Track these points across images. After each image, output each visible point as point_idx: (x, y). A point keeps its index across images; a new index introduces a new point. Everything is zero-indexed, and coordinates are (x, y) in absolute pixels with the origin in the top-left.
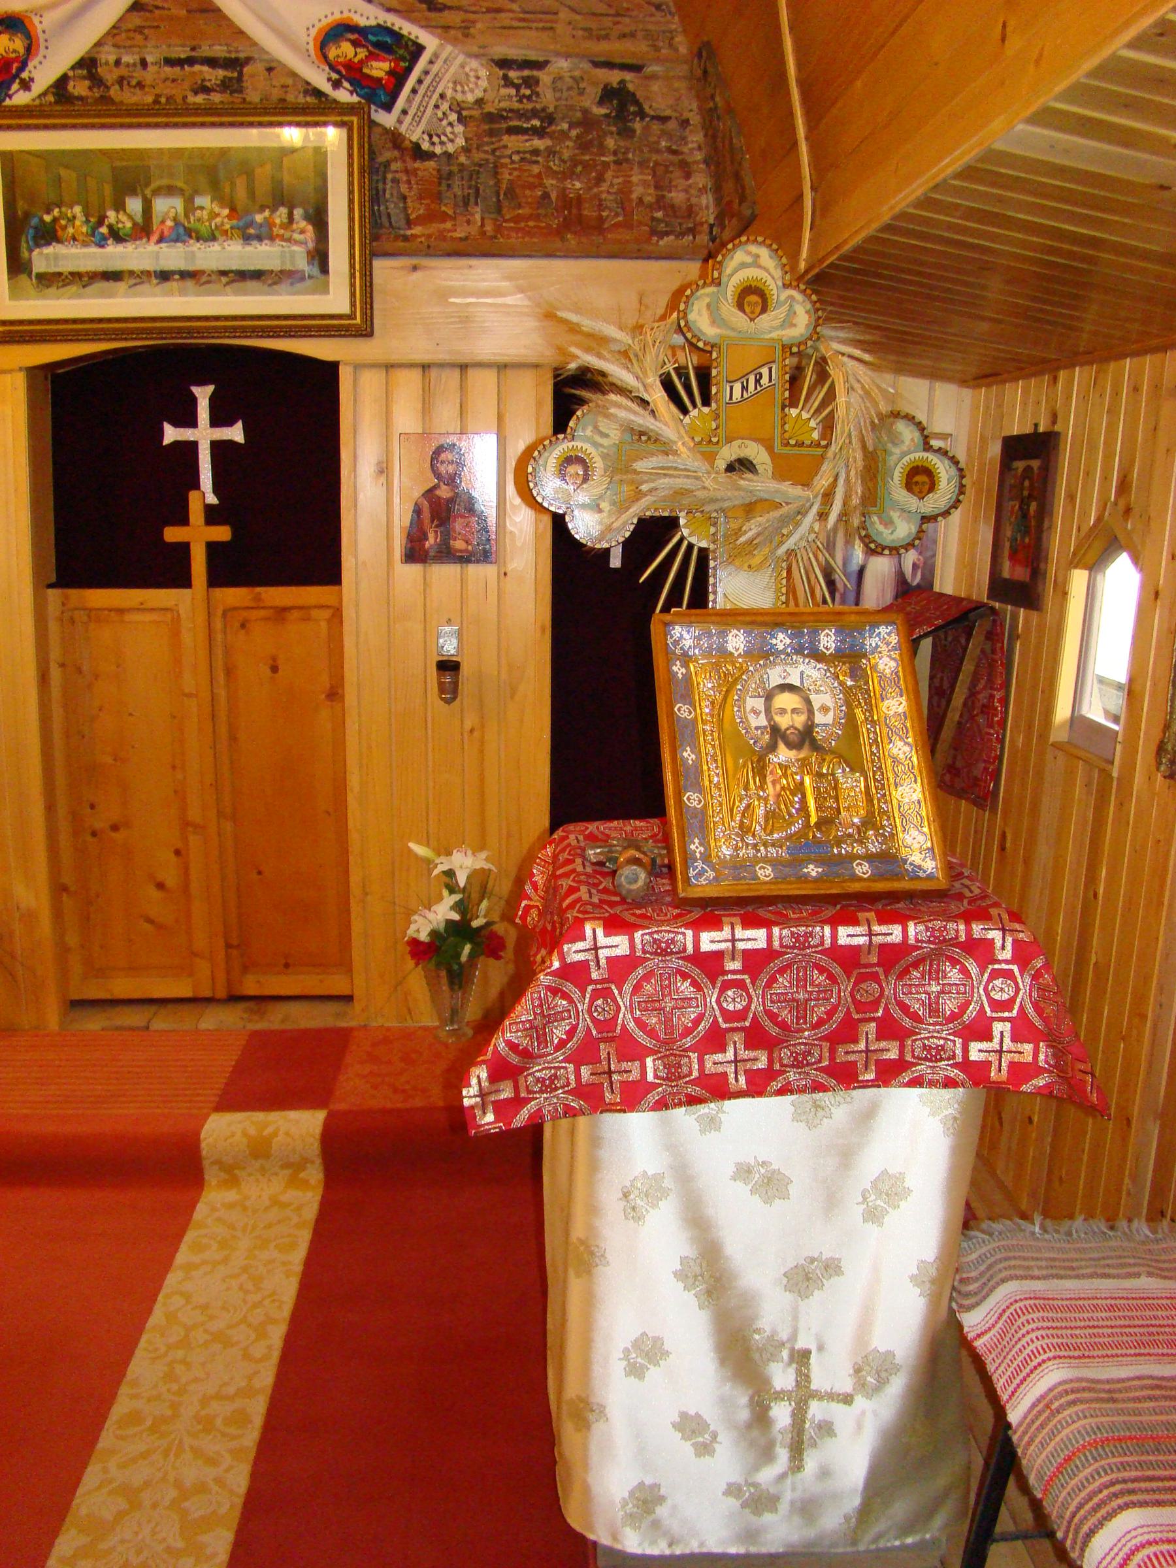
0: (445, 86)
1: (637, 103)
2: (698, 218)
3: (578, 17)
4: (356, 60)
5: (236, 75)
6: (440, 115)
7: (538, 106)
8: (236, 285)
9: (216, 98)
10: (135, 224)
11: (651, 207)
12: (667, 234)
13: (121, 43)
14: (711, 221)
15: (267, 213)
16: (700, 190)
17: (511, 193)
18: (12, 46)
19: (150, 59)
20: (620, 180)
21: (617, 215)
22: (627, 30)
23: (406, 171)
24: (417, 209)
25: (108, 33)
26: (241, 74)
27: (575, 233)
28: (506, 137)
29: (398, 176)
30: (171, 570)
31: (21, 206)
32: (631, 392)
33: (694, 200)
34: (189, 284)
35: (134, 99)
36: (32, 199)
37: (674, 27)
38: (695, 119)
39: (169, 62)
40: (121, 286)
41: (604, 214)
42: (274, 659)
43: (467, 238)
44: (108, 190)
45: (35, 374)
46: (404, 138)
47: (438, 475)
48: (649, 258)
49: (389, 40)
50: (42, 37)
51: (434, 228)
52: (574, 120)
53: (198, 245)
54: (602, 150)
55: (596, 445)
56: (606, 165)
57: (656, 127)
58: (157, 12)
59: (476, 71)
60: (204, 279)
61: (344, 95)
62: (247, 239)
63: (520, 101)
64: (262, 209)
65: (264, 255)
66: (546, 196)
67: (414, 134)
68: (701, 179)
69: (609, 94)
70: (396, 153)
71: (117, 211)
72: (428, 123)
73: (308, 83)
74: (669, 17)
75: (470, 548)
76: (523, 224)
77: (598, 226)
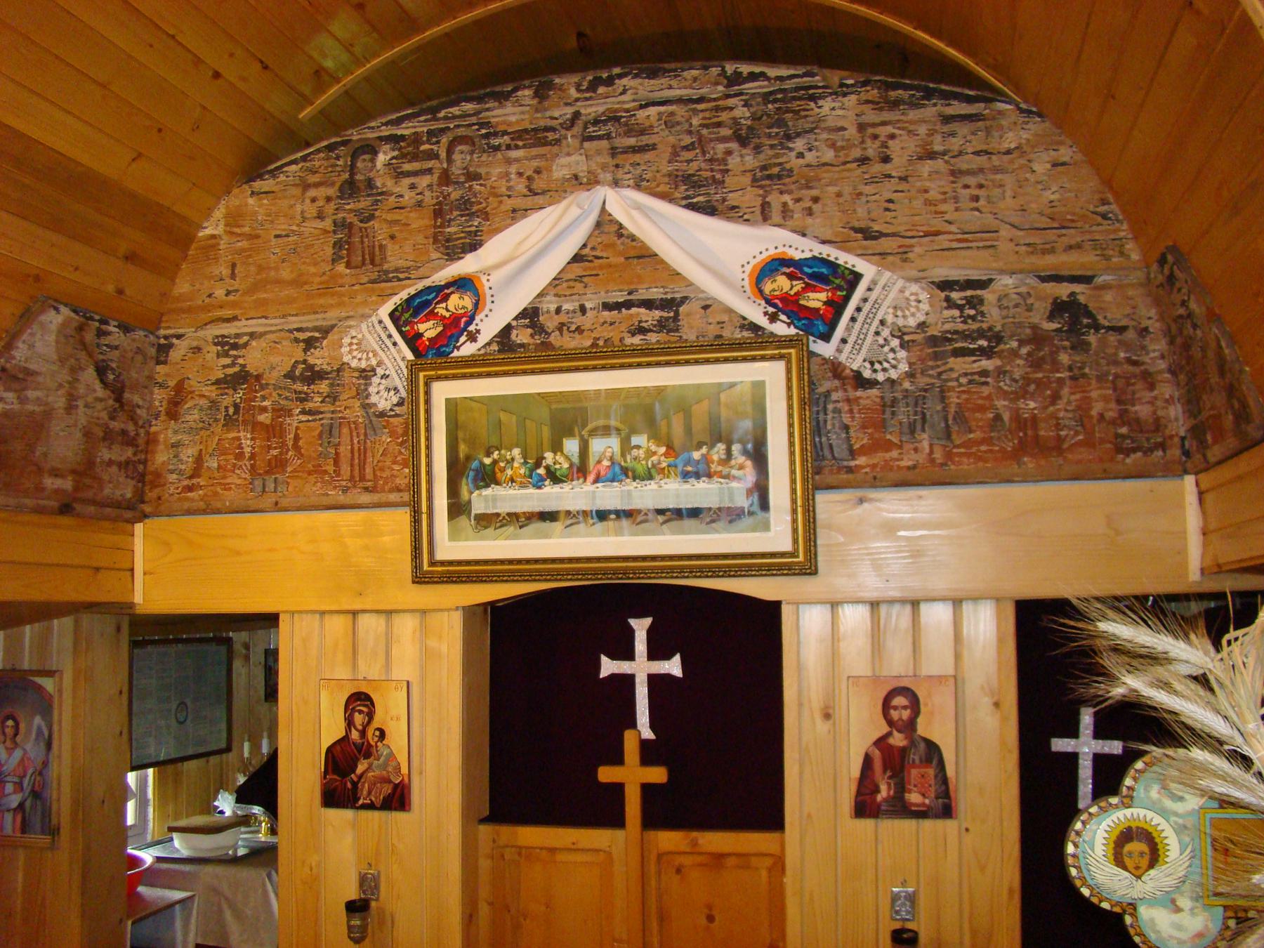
0: (885, 312)
1: (1089, 314)
2: (1167, 432)
3: (1021, 233)
4: (792, 293)
5: (672, 314)
6: (881, 341)
7: (985, 326)
8: (673, 523)
9: (653, 338)
10: (571, 465)
11: (1113, 422)
12: (1134, 450)
13: (561, 293)
14: (1182, 434)
15: (704, 450)
16: (1167, 401)
17: (960, 417)
18: (461, 303)
19: (588, 305)
20: (1078, 396)
21: (1077, 433)
22: (1073, 242)
23: (848, 400)
24: (860, 439)
25: (550, 284)
26: (677, 313)
27: (1032, 456)
28: (952, 360)
29: (839, 405)
30: (603, 809)
31: (463, 449)
32: (1221, 743)
33: (1160, 413)
34: (625, 523)
35: (573, 344)
36: (472, 442)
37: (1122, 234)
38: (1155, 326)
39: (607, 307)
40: (558, 526)
41: (1063, 433)
42: (710, 907)
43: (914, 467)
44: (546, 432)
45: (470, 613)
46: (845, 367)
47: (890, 722)
48: (1115, 478)
49: (824, 270)
50: (488, 293)
51: (879, 458)
52: (1023, 337)
53: (635, 484)
54: (1056, 366)
55: (1163, 813)
56: (1061, 381)
57: (1112, 338)
58: (597, 262)
59: (916, 294)
60: (640, 518)
61: (781, 329)
62: (686, 476)
63: (965, 322)
64: (699, 447)
65: (702, 493)
66: (998, 418)
67: (856, 363)
68: (1166, 390)
69: (1058, 308)
70: (837, 383)
71: (555, 453)
72: (869, 350)
73: (744, 319)
74: (1117, 225)
75: (927, 801)
76: (974, 449)
77: (1057, 447)
